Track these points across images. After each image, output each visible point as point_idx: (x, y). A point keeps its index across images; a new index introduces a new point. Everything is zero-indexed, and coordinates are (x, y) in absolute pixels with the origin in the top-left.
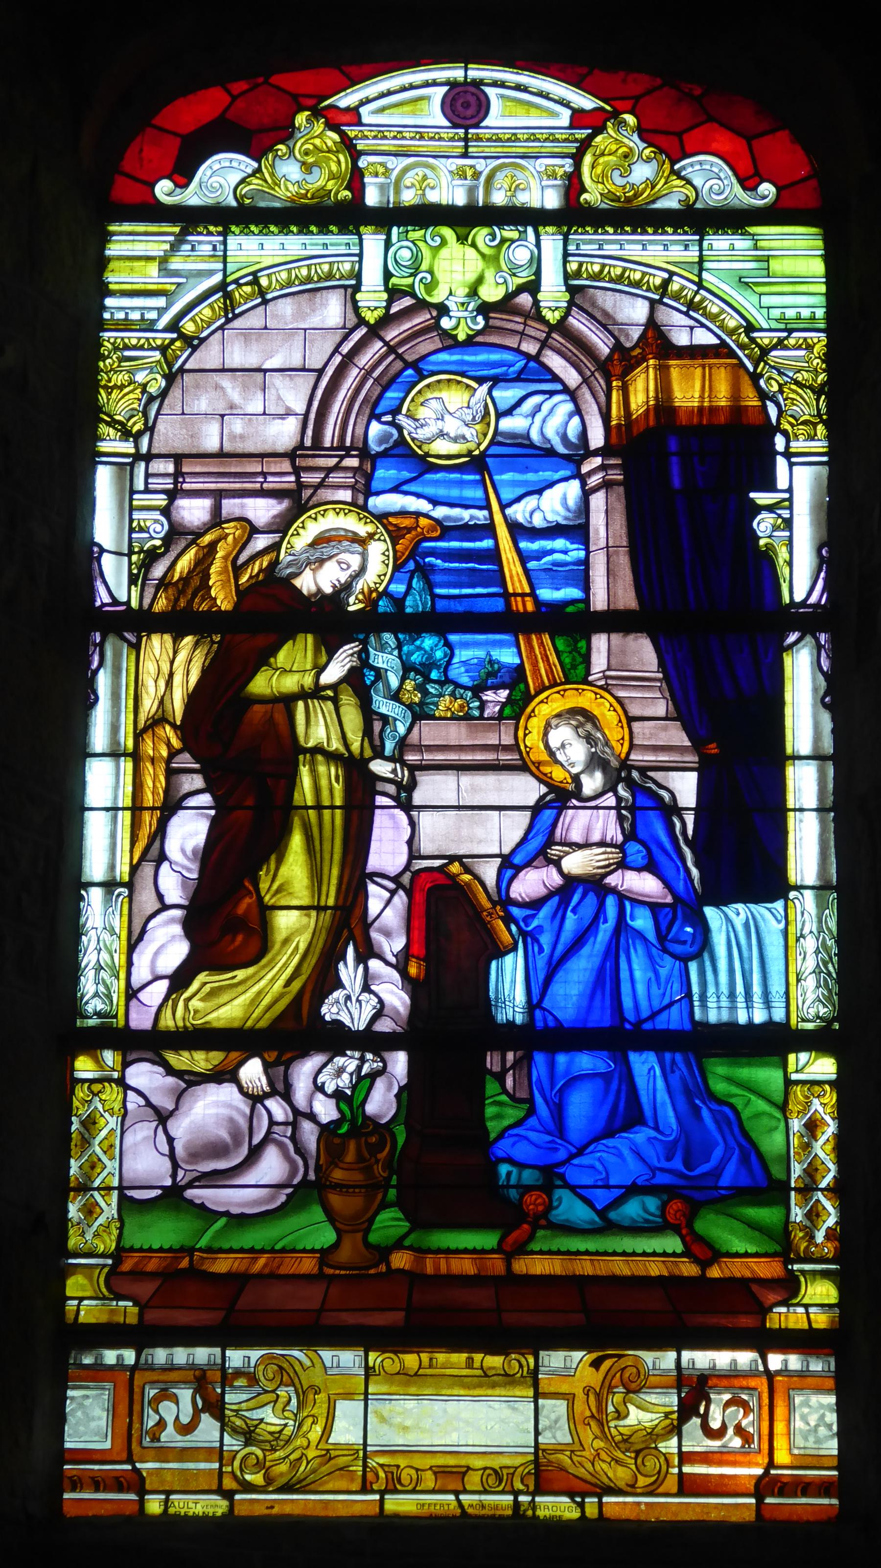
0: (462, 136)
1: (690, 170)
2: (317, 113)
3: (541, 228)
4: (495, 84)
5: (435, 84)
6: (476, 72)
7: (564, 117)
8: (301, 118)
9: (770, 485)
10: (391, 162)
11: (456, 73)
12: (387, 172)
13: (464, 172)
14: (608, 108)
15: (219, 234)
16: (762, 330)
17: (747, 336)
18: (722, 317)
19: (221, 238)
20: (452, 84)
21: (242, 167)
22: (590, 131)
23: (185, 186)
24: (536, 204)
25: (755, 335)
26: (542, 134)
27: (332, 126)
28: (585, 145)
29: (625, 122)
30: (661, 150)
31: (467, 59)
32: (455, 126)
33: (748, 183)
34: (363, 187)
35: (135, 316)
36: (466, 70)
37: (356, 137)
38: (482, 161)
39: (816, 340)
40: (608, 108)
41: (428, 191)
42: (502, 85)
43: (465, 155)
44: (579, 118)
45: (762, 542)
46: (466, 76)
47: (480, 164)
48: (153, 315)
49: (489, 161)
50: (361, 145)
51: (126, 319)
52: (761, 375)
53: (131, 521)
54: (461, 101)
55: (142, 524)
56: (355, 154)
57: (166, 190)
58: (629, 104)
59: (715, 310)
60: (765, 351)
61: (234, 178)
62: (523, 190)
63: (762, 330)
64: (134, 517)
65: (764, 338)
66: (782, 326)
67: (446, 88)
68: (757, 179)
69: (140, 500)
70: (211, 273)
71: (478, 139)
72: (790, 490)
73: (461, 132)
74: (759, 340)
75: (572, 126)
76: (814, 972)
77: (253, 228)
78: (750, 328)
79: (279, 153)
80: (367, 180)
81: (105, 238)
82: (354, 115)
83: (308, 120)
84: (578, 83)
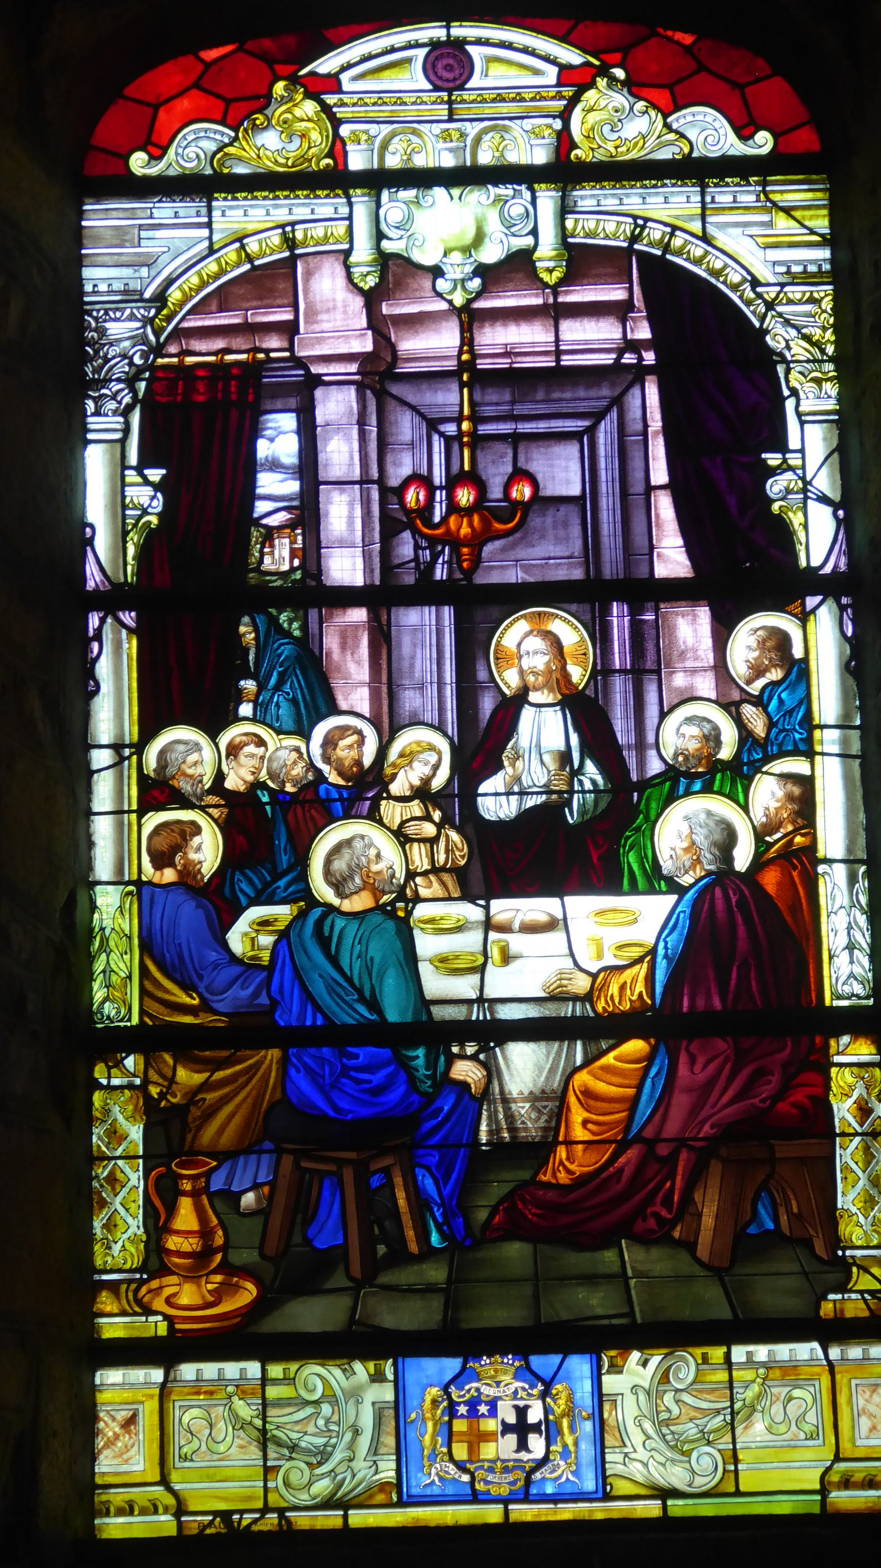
0: (446, 98)
1: (682, 121)
2: (294, 80)
3: (536, 186)
4: (479, 42)
5: (417, 45)
6: (458, 31)
7: (551, 74)
8: (279, 88)
9: (782, 446)
10: (373, 129)
11: (435, 32)
12: (463, 135)
13: (450, 135)
14: (597, 63)
15: (757, 183)
16: (768, 285)
17: (753, 289)
18: (187, 289)
20: (434, 45)
21: (218, 137)
23: (160, 158)
24: (525, 160)
25: (759, 289)
26: (370, 99)
27: (312, 94)
28: (574, 101)
31: (448, 18)
32: (436, 89)
33: (744, 133)
34: (345, 154)
36: (448, 27)
37: (335, 105)
40: (597, 63)
42: (486, 43)
43: (451, 120)
45: (776, 507)
46: (449, 35)
50: (340, 113)
53: (124, 497)
55: (136, 501)
57: (140, 163)
58: (617, 57)
59: (195, 280)
60: (770, 306)
62: (418, 153)
63: (768, 285)
65: (770, 293)
67: (426, 50)
68: (752, 128)
71: (463, 101)
72: (802, 451)
73: (444, 95)
74: (766, 296)
75: (559, 84)
76: (847, 948)
78: (755, 283)
79: (258, 122)
81: (81, 215)
82: (332, 83)
83: (286, 88)
84: (564, 38)
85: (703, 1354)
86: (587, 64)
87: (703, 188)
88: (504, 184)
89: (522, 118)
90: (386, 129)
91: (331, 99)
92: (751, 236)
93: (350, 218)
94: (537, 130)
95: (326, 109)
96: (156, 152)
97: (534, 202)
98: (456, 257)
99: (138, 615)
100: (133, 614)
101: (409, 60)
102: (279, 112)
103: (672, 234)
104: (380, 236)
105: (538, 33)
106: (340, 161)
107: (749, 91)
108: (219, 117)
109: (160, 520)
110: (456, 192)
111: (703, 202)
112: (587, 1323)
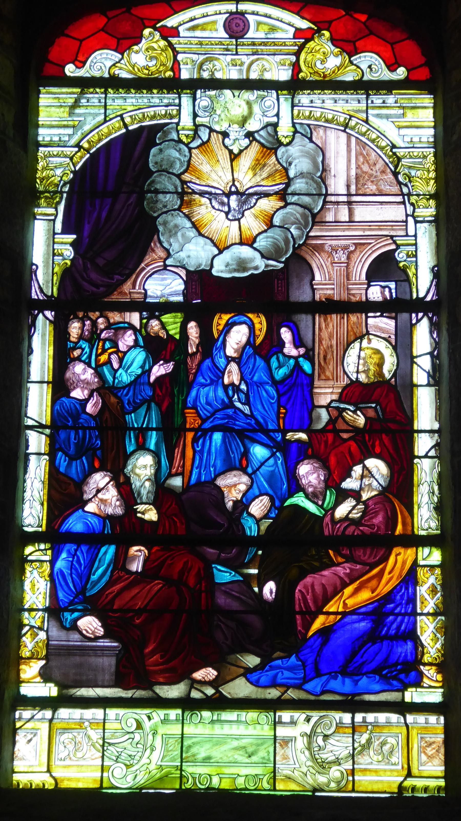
4: (253, 13)
6: (243, 7)
11: (232, 7)
19: (104, 96)
21: (113, 58)
22: (303, 40)
24: (275, 78)
25: (394, 150)
27: (164, 37)
28: (302, 47)
29: (323, 35)
30: (344, 50)
32: (231, 37)
33: (392, 68)
34: (180, 70)
35: (56, 139)
37: (176, 44)
38: (245, 56)
39: (428, 153)
41: (215, 72)
44: (298, 33)
45: (401, 265)
47: (244, 58)
48: (66, 138)
49: (249, 56)
50: (178, 48)
51: (51, 141)
52: (399, 173)
53: (54, 250)
54: (234, 25)
56: (176, 53)
57: (71, 70)
61: (109, 64)
62: (267, 71)
64: (55, 247)
66: (412, 146)
68: (397, 66)
69: (59, 238)
70: (97, 115)
71: (244, 45)
72: (415, 236)
74: (398, 154)
75: (295, 38)
77: (120, 90)
80: (182, 66)
82: (174, 32)
85: (291, 716)
86: (310, 28)
87: (368, 95)
88: (302, 90)
89: (274, 55)
90: (202, 58)
91: (174, 40)
92: (392, 122)
93: (180, 105)
94: (282, 62)
95: (171, 45)
96: (81, 65)
97: (278, 99)
98: (236, 127)
99: (55, 314)
100: (53, 313)
101: (215, 22)
102: (144, 44)
103: (350, 119)
104: (195, 115)
105: (283, 9)
106: (177, 73)
107: (397, 46)
108: (115, 48)
109: (71, 263)
110: (237, 93)
111: (367, 103)
112: (128, 694)
